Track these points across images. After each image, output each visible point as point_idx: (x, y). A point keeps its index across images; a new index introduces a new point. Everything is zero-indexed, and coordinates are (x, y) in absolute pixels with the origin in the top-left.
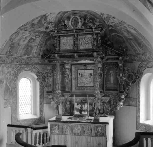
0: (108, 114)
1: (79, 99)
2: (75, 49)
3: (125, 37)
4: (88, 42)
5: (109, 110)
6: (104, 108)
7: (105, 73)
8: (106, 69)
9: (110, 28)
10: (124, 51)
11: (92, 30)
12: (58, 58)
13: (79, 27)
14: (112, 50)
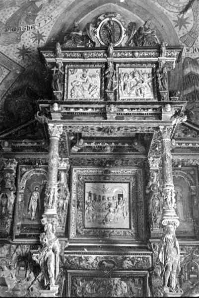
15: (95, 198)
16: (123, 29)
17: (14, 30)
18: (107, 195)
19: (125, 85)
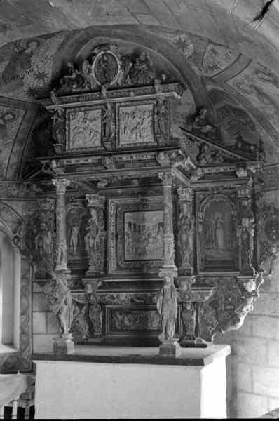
0: (209, 340)
1: (125, 294)
2: (108, 145)
3: (252, 109)
5: (213, 327)
6: (197, 321)
7: (200, 220)
8: (203, 207)
9: (210, 87)
10: (250, 151)
11: (154, 88)
12: (61, 171)
15: (135, 228)
16: (119, 62)
18: (147, 224)
19: (125, 128)
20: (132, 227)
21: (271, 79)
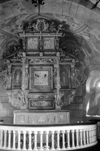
4: (51, 43)
13: (44, 31)
14: (66, 53)
17: (9, 25)
20: (36, 76)
21: (88, 35)
